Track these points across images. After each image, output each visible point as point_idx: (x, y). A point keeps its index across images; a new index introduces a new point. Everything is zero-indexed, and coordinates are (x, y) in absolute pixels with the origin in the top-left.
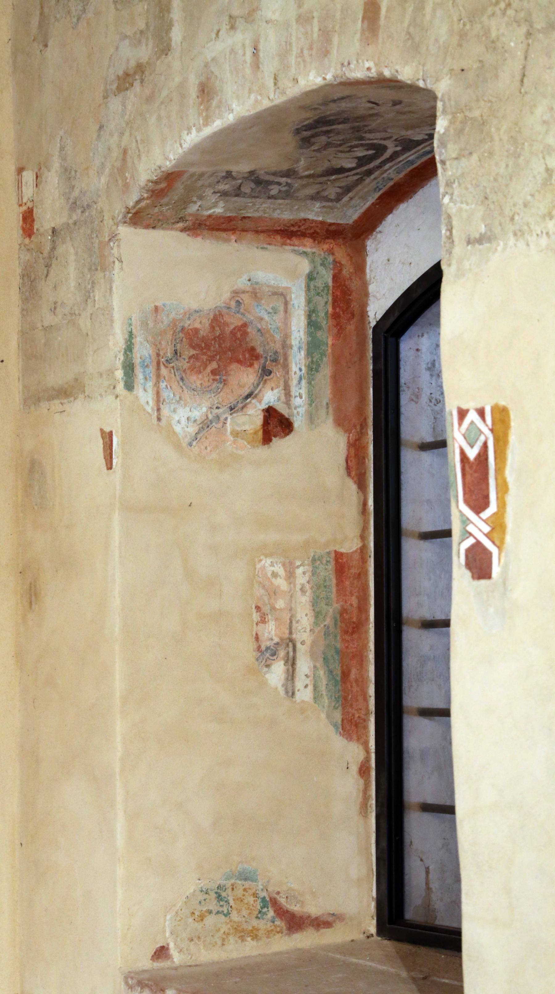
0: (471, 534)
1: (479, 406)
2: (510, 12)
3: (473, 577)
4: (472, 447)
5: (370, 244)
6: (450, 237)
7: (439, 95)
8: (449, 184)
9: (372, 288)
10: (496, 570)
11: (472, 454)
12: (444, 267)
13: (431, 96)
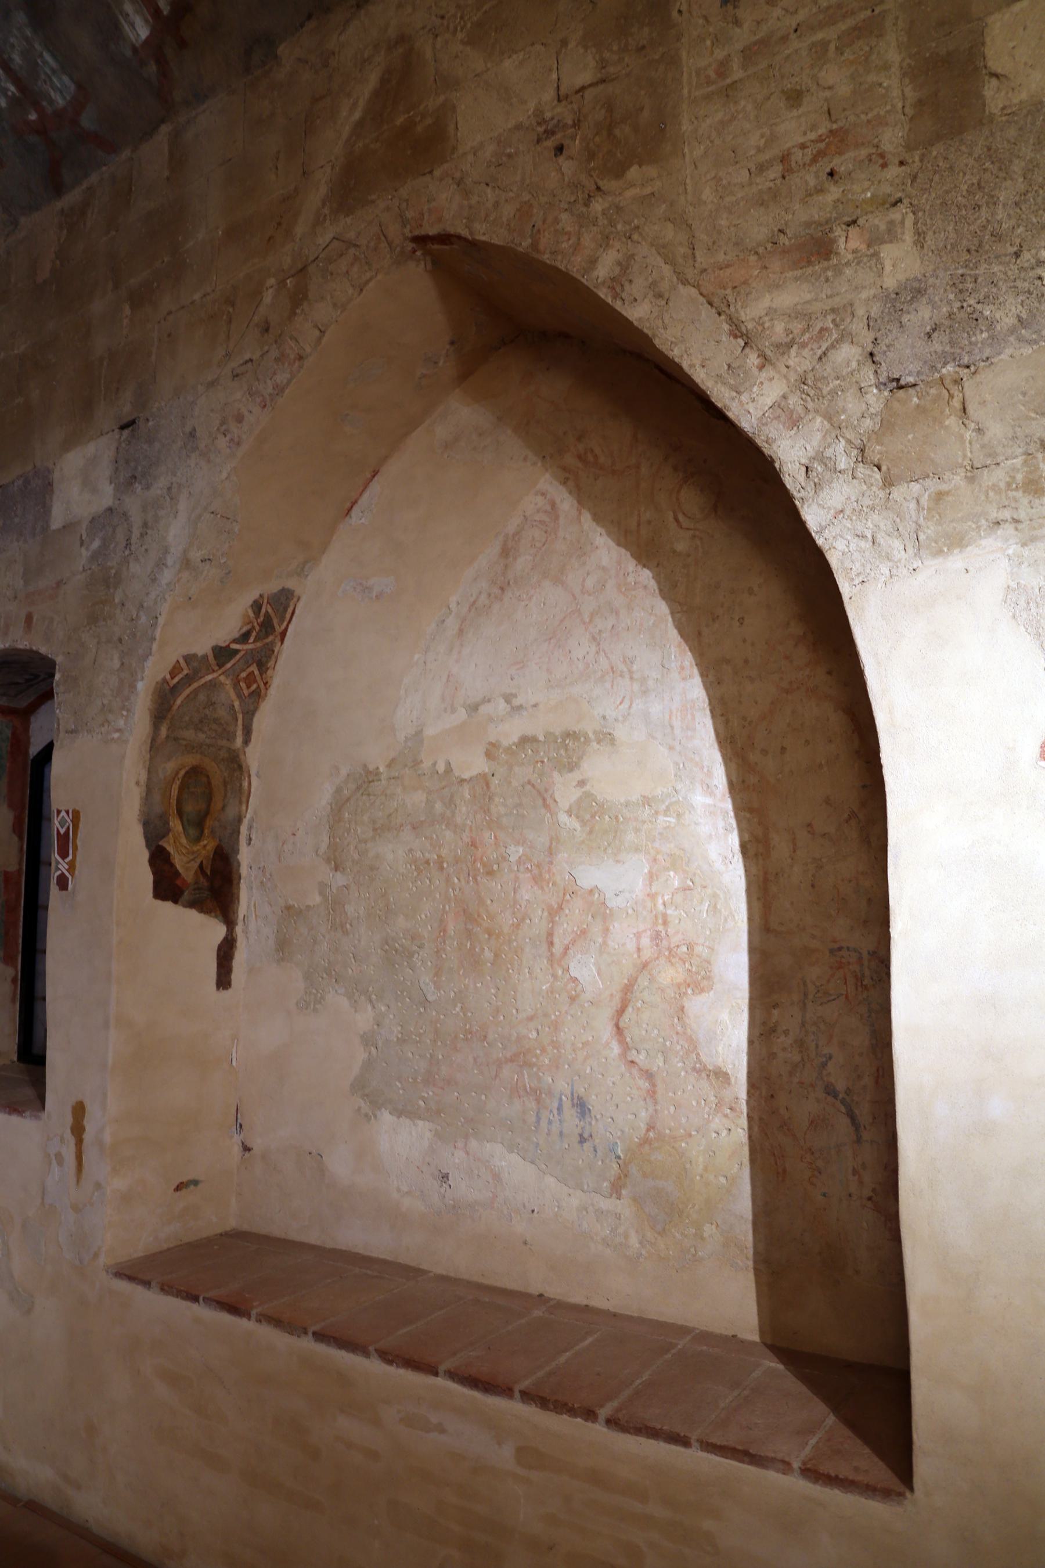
0: (60, 869)
1: (67, 808)
2: (91, 632)
3: (60, 890)
4: (62, 828)
5: (32, 719)
6: (58, 729)
7: (57, 663)
8: (59, 704)
9: (32, 740)
10: (70, 886)
11: (62, 831)
12: (55, 742)
13: (52, 664)
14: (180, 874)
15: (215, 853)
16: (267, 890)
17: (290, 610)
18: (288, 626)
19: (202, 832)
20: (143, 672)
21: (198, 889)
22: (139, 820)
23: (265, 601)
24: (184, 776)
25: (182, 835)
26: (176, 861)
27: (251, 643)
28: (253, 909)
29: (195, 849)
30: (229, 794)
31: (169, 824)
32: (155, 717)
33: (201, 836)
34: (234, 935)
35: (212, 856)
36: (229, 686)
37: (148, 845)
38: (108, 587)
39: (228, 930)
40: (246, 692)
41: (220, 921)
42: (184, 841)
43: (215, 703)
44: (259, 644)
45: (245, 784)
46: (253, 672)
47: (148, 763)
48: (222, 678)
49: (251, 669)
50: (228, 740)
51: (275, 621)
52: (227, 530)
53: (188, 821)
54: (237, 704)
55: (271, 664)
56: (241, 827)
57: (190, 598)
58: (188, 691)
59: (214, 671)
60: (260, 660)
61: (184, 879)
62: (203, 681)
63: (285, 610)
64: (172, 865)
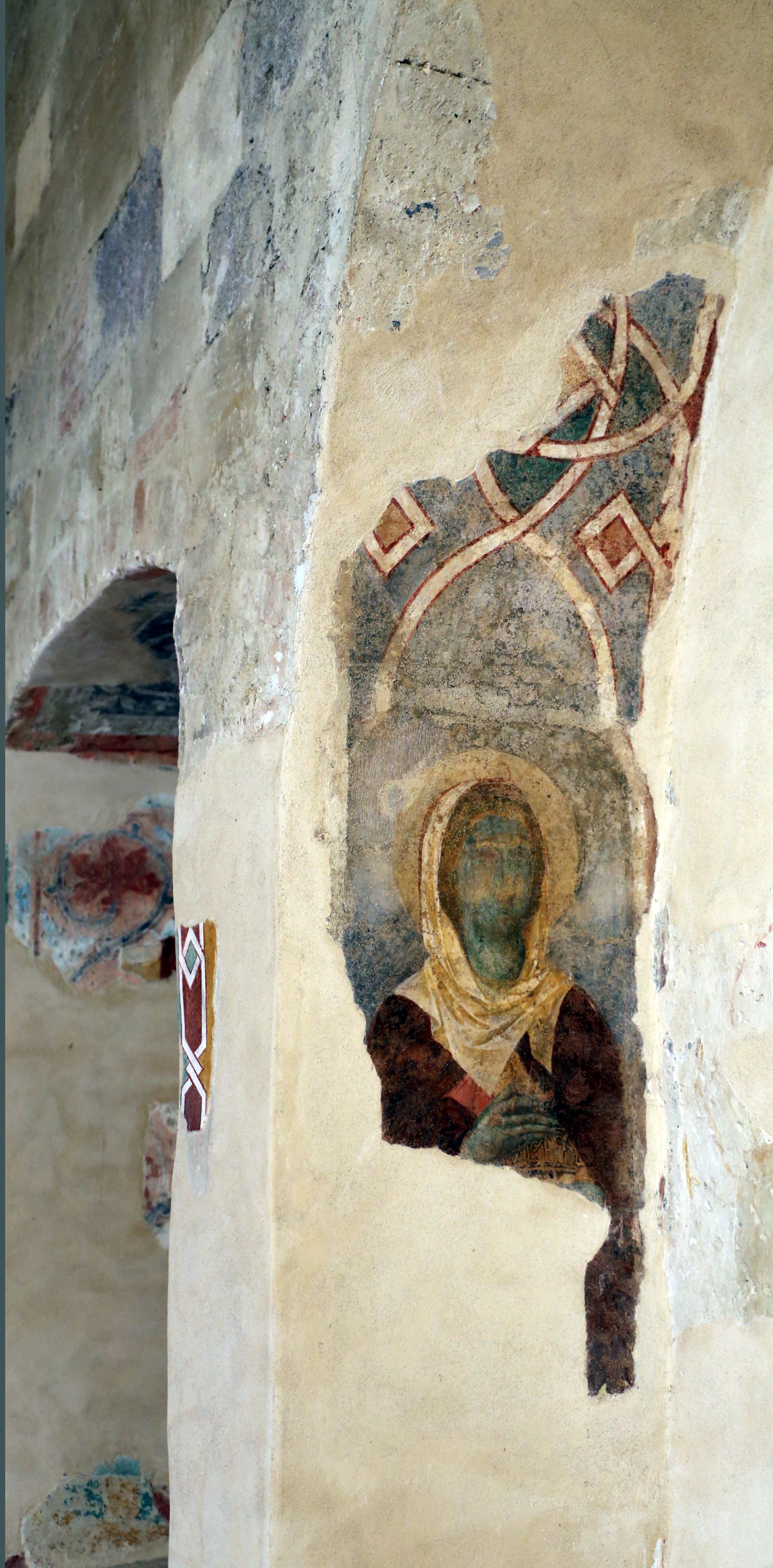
14: (463, 1073)
15: (565, 1010)
16: (710, 1105)
17: (701, 339)
18: (701, 383)
19: (523, 955)
20: (303, 539)
21: (519, 1110)
22: (330, 932)
23: (622, 317)
24: (458, 809)
25: (463, 967)
26: (448, 1036)
27: (600, 439)
28: (681, 1161)
29: (504, 1002)
30: (593, 854)
31: (421, 939)
32: (353, 656)
33: (521, 966)
34: (635, 1236)
35: (554, 1020)
36: (555, 561)
37: (362, 996)
38: (244, 361)
39: (615, 1223)
40: (610, 576)
41: (592, 1199)
42: (467, 981)
43: (521, 610)
44: (624, 441)
45: (639, 823)
46: (619, 518)
47: (345, 779)
48: (532, 541)
49: (612, 511)
50: (576, 707)
51: (663, 374)
52: (460, 111)
53: (477, 927)
54: (586, 609)
55: (670, 493)
56: (638, 938)
57: (397, 324)
58: (437, 582)
59: (505, 524)
60: (637, 485)
61: (474, 1086)
62: (477, 552)
63: (686, 339)
64: (437, 1049)
